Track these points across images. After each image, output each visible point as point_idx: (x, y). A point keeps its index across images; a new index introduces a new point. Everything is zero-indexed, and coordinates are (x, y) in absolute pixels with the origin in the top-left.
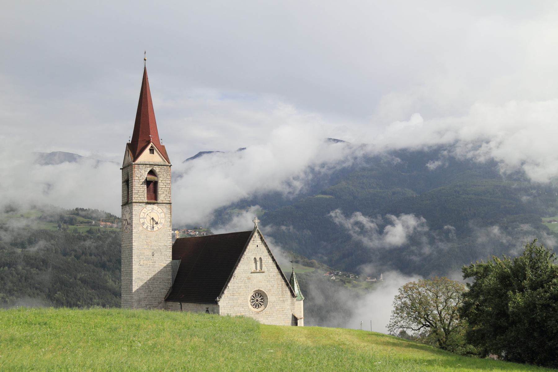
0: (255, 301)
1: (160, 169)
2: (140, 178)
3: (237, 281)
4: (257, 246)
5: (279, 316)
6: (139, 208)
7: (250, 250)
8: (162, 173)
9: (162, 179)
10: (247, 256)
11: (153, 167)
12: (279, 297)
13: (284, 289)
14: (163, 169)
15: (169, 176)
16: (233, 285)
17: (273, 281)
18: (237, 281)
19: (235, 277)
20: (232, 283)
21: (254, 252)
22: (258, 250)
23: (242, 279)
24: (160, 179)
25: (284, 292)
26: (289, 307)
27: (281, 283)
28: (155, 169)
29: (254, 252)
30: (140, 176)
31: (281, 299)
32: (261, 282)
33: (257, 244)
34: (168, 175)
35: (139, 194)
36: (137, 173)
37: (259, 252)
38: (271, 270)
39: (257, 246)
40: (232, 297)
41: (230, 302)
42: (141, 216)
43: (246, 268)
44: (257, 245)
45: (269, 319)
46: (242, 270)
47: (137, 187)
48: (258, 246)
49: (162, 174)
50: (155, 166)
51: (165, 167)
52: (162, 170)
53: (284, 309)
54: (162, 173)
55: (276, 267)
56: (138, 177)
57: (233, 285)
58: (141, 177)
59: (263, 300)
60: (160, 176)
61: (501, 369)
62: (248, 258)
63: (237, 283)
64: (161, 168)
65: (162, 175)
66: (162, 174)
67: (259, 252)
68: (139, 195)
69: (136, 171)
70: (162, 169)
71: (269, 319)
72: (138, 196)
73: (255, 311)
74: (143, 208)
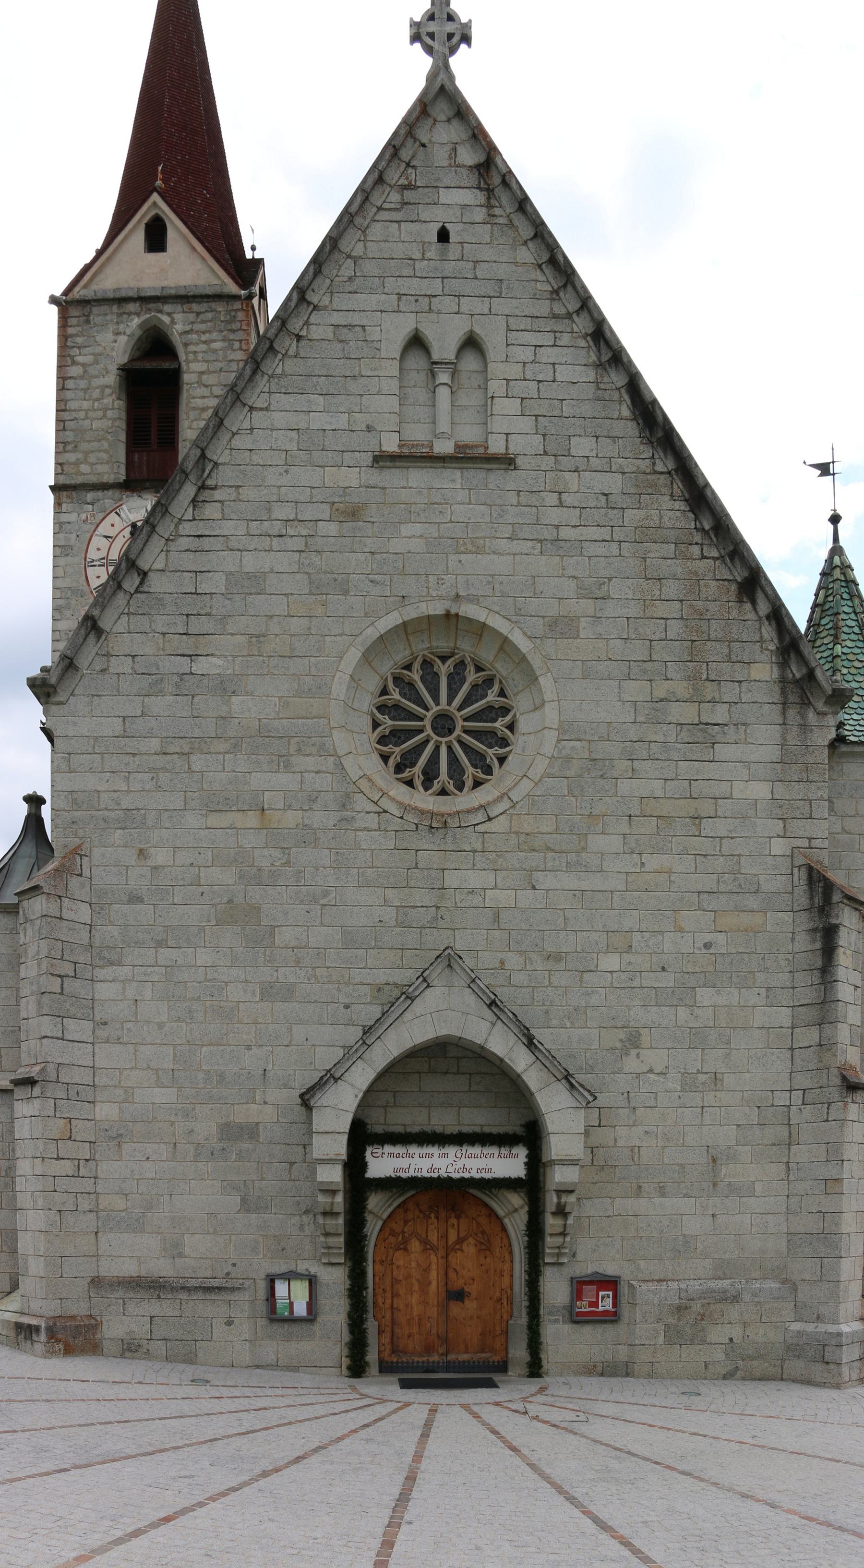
0: (437, 748)
1: (192, 317)
2: (92, 371)
3: (227, 528)
4: (443, 236)
5: (653, 862)
6: (84, 516)
7: (369, 267)
8: (204, 338)
9: (203, 367)
10: (337, 318)
11: (160, 312)
12: (661, 689)
13: (716, 629)
14: (209, 315)
15: (241, 349)
16: (190, 562)
17: (599, 549)
18: (227, 528)
19: (206, 495)
20: (184, 543)
21: (414, 286)
22: (449, 268)
23: (283, 512)
24: (195, 367)
25: (715, 651)
26: (760, 790)
27: (677, 567)
28: (166, 319)
29: (414, 286)
30: (89, 359)
31: (688, 714)
32: (479, 551)
33: (437, 216)
34: (237, 345)
35: (84, 446)
36: (79, 348)
37: (454, 285)
38: (582, 446)
39: (443, 236)
40: (184, 664)
41: (157, 704)
42: (93, 554)
43: (318, 421)
44: (436, 227)
45: (546, 880)
46: (289, 441)
47: (74, 415)
48: (452, 238)
49: (205, 342)
50: (167, 308)
51: (220, 307)
52: (203, 322)
53: (706, 808)
54: (204, 338)
55: (630, 429)
56: (83, 365)
57: (190, 562)
58: (96, 362)
59: (444, 659)
60: (195, 353)
61: (350, 1290)
62: (345, 334)
63: (233, 543)
64: (198, 314)
65: (203, 347)
66: (205, 342)
67: (454, 285)
68: (87, 453)
69: (72, 336)
70: (202, 317)
71: (546, 880)
72: (80, 456)
73: (406, 808)
74: (101, 516)
